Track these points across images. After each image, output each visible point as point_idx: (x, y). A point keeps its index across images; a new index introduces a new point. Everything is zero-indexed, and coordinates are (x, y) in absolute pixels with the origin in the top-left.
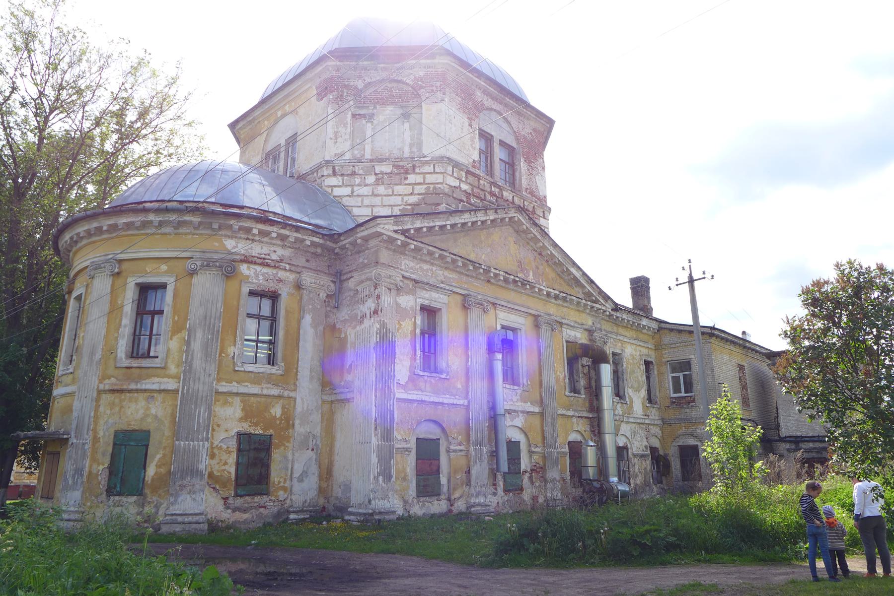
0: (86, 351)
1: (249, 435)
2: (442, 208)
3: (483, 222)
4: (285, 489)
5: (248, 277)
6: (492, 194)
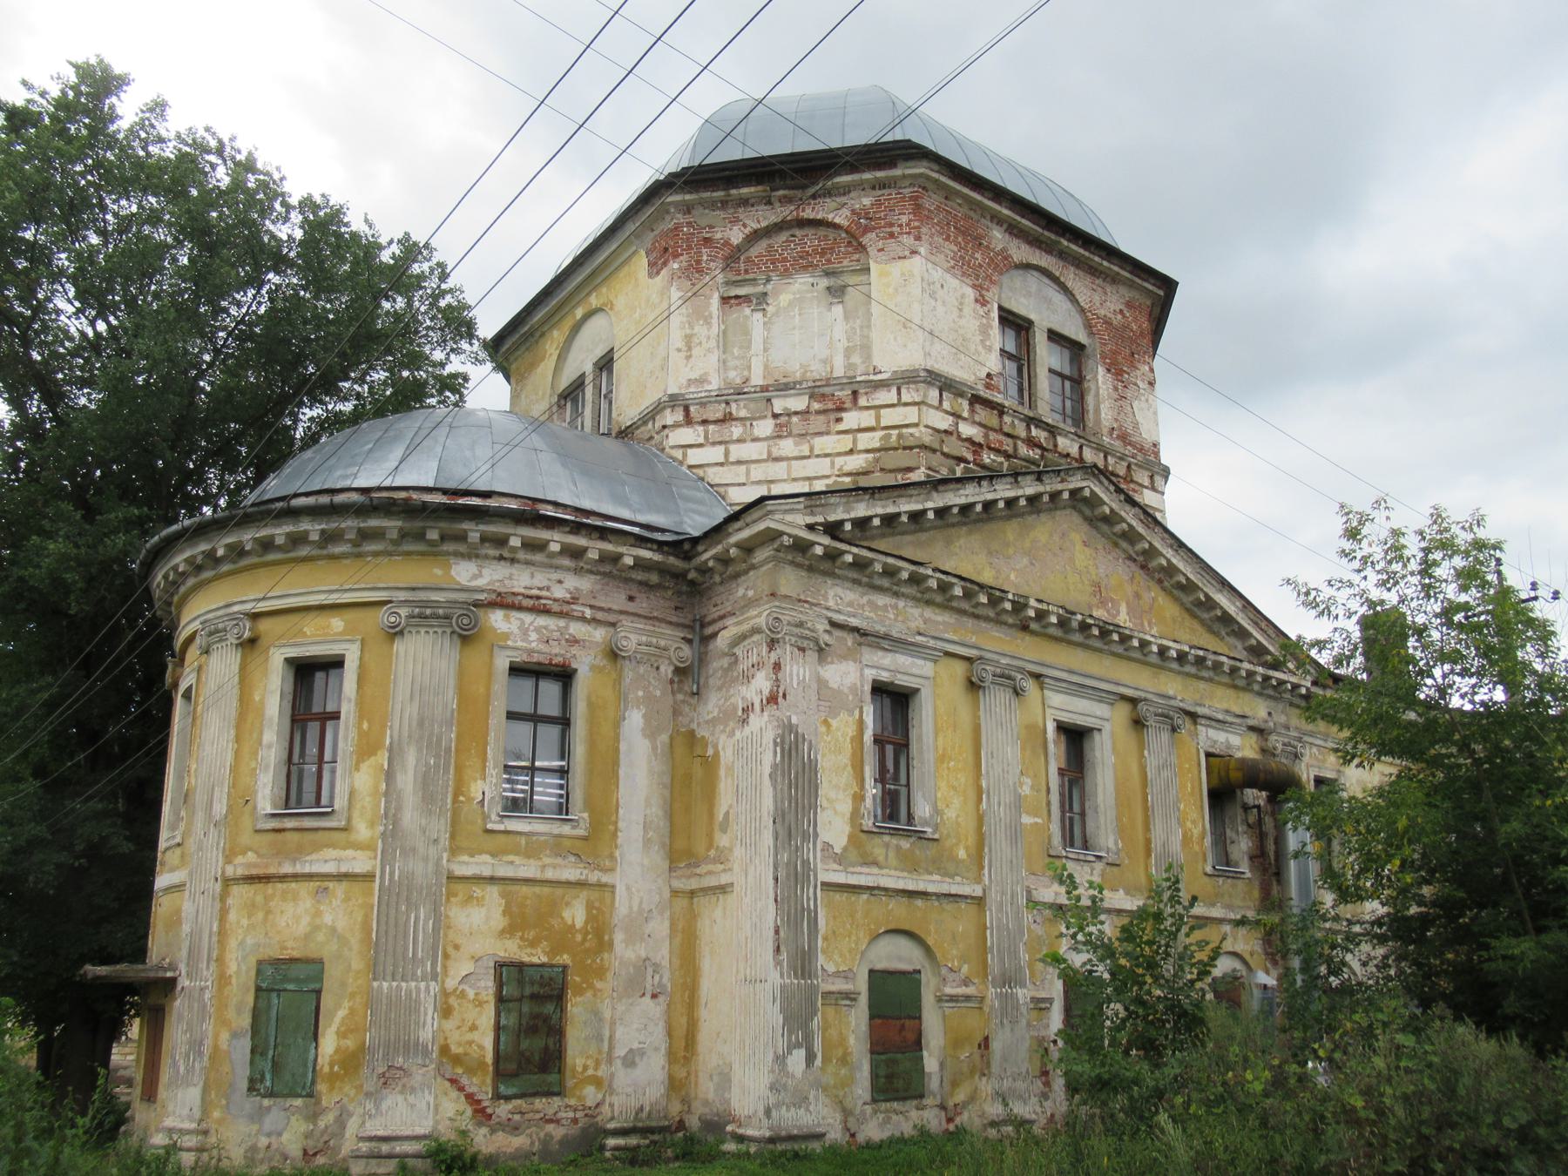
0: (199, 798)
1: (520, 966)
2: (918, 476)
3: (1010, 503)
4: (597, 1082)
5: (506, 636)
6: (1032, 443)
